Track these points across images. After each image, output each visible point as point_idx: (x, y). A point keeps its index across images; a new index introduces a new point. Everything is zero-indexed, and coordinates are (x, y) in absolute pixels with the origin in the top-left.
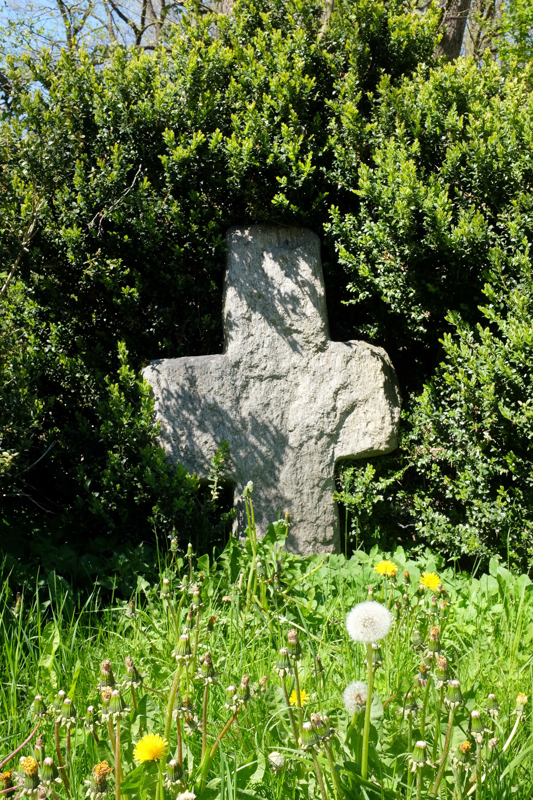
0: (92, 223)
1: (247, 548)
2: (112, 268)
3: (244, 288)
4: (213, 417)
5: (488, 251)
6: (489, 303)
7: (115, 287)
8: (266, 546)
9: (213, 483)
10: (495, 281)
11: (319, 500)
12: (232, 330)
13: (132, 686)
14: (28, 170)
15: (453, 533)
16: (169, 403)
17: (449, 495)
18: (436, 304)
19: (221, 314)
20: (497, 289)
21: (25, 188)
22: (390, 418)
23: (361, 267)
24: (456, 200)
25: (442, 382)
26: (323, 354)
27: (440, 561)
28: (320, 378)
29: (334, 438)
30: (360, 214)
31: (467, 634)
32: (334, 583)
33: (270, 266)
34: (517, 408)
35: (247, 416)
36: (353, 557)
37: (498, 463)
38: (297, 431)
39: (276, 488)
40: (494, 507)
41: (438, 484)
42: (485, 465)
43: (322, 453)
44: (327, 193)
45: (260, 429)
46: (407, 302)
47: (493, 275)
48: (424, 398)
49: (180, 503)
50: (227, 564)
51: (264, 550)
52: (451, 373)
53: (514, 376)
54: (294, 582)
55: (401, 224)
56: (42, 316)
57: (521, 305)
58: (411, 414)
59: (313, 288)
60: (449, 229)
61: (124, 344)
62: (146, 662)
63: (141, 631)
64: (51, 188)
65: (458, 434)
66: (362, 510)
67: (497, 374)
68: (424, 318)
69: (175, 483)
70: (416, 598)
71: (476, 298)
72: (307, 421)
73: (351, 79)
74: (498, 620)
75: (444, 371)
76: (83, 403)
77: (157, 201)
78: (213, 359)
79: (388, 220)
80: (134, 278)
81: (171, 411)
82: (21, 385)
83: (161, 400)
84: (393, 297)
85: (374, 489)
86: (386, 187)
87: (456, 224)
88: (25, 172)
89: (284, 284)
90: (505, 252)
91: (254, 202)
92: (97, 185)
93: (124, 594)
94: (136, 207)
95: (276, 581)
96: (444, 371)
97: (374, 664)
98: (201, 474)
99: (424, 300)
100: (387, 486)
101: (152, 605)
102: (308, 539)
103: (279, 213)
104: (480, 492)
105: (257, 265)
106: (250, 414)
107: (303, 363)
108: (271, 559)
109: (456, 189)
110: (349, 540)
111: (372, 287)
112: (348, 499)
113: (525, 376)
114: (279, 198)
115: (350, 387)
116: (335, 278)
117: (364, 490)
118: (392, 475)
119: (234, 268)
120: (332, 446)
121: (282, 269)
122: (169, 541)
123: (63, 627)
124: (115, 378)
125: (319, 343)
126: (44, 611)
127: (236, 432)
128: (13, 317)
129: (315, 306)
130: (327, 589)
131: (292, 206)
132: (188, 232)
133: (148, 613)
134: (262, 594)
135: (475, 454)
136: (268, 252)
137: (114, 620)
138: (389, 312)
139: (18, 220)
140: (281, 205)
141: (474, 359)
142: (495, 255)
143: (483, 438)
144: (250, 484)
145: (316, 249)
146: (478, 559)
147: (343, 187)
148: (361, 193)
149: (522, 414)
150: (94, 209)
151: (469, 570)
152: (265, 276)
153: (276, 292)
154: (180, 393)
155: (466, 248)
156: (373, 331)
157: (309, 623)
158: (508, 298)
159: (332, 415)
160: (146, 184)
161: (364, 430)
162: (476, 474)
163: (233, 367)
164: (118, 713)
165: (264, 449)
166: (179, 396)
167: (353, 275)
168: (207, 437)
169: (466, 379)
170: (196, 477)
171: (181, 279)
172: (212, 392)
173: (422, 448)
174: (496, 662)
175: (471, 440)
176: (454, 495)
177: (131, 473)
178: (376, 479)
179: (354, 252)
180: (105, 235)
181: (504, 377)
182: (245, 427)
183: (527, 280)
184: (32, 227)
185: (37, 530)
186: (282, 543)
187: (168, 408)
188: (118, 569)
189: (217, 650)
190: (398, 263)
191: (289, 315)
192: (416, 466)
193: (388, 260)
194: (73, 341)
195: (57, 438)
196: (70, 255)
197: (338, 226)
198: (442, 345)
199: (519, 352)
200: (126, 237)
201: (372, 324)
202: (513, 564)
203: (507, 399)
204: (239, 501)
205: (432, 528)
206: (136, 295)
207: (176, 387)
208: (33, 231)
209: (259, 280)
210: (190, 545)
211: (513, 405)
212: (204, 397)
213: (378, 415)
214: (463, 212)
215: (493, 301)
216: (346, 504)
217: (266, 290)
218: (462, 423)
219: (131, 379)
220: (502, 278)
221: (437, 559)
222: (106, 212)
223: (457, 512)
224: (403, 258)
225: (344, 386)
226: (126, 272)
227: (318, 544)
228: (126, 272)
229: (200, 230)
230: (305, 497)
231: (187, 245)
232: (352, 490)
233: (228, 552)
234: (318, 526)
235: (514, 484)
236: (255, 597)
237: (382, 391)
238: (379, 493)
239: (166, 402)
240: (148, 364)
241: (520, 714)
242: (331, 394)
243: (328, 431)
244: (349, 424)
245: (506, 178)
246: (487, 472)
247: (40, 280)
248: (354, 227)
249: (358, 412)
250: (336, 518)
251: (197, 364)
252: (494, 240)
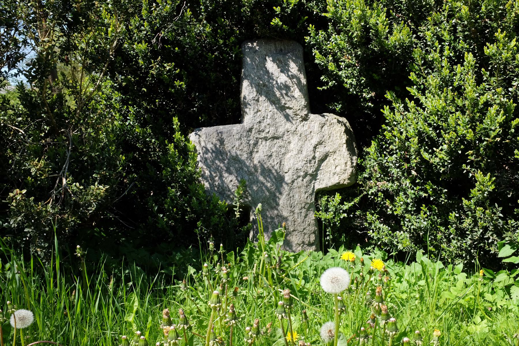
0: (154, 41)
1: (258, 247)
2: (168, 69)
3: (254, 81)
4: (236, 164)
5: (413, 51)
6: (414, 85)
7: (170, 81)
8: (271, 246)
9: (236, 207)
10: (418, 70)
11: (305, 217)
12: (247, 108)
13: (184, 327)
14: (111, 5)
15: (393, 237)
16: (207, 156)
17: (389, 212)
18: (378, 86)
19: (239, 98)
20: (419, 76)
21: (110, 18)
22: (350, 163)
23: (330, 64)
24: (391, 19)
25: (384, 139)
26: (306, 122)
27: (384, 255)
28: (305, 138)
29: (314, 176)
30: (329, 31)
31: (402, 300)
32: (316, 270)
33: (271, 66)
34: (433, 153)
35: (257, 163)
36: (328, 254)
37: (421, 190)
38: (290, 173)
39: (277, 210)
40: (419, 218)
41: (382, 206)
42: (413, 192)
43: (307, 187)
44: (306, 17)
45: (266, 172)
46: (360, 87)
47: (416, 67)
48: (372, 149)
49: (215, 219)
50: (246, 258)
51: (269, 248)
52: (390, 132)
53: (431, 132)
54: (289, 268)
55: (355, 35)
56: (124, 102)
57: (434, 85)
58: (364, 160)
60: (387, 38)
61: (177, 118)
62: (194, 318)
63: (191, 300)
64: (127, 17)
65: (394, 171)
66: (333, 223)
67: (419, 131)
68: (372, 96)
69: (211, 207)
70: (368, 276)
71: (405, 83)
72: (296, 166)
74: (423, 291)
75: (385, 130)
76: (151, 157)
77: (196, 25)
78: (235, 127)
79: (347, 32)
80: (182, 75)
81: (208, 161)
82: (111, 145)
83: (201, 154)
84: (351, 84)
85: (341, 209)
86: (344, 11)
87: (391, 34)
88: (110, 6)
89: (280, 77)
90: (424, 52)
91: (259, 24)
92: (157, 15)
93: (179, 277)
94: (183, 24)
95: (277, 267)
96: (385, 130)
97: (339, 309)
98: (228, 201)
99: (371, 85)
100: (349, 208)
101: (198, 283)
102: (299, 242)
103: (276, 31)
104: (410, 209)
105: (262, 65)
106: (259, 162)
107: (293, 129)
108: (275, 254)
109: (391, 11)
110: (325, 243)
111: (337, 78)
112: (324, 216)
113: (438, 131)
114: (276, 21)
115: (324, 143)
116: (313, 72)
117: (334, 210)
118: (353, 200)
119: (247, 67)
120: (313, 182)
121: (279, 67)
122: (208, 243)
123: (141, 299)
124: (171, 141)
125: (303, 115)
126: (128, 289)
127: (251, 174)
128: (105, 103)
129: (300, 91)
130: (311, 273)
131: (284, 26)
132: (217, 45)
133: (196, 289)
134: (269, 276)
135: (406, 185)
136: (269, 57)
137: (174, 294)
138: (349, 93)
139: (107, 39)
140: (277, 25)
141: (404, 122)
142: (417, 53)
143: (411, 174)
144: (260, 206)
145: (300, 54)
146: (409, 253)
147: (317, 13)
148: (329, 15)
149: (436, 156)
150: (155, 31)
151: (403, 261)
152: (268, 72)
153: (275, 82)
154: (214, 149)
155: (398, 49)
157: (300, 294)
158: (426, 81)
159: (313, 162)
160: (189, 13)
161: (333, 171)
162: (407, 197)
163: (248, 131)
164: (174, 340)
165: (269, 185)
166: (213, 151)
167: (325, 71)
168: (232, 177)
169: (399, 135)
170: (225, 203)
171: (213, 75)
172: (235, 148)
173: (372, 182)
174: (421, 316)
175: (403, 175)
176: (393, 212)
177: (183, 201)
178: (342, 203)
179: (325, 55)
180: (163, 48)
181: (423, 133)
182: (256, 171)
183: (438, 69)
184: (115, 42)
185: (124, 239)
186: (281, 243)
187: (206, 159)
188: (176, 262)
189: (240, 311)
190: (354, 61)
191: (283, 97)
192: (368, 194)
193: (347, 59)
194: (144, 118)
195: (135, 181)
196: (141, 62)
197: (314, 38)
198: (384, 114)
199: (434, 116)
200: (177, 49)
201: (338, 103)
202: (432, 255)
203: (426, 147)
204: (253, 219)
205: (378, 234)
206: (184, 86)
207: (211, 146)
208: (116, 45)
209: (264, 75)
210: (221, 245)
211: (430, 151)
212: (230, 152)
213: (343, 161)
214: (395, 26)
215: (417, 84)
216: (323, 219)
217: (269, 82)
218: (397, 165)
219: (182, 141)
220: (422, 68)
221: (383, 254)
222: (163, 33)
223: (395, 223)
224: (357, 57)
225: (320, 143)
226: (177, 72)
227: (305, 246)
228: (177, 72)
229: (224, 43)
230: (296, 215)
231: (216, 53)
232: (327, 210)
233: (247, 250)
234: (305, 234)
235: (432, 203)
236: (265, 278)
237: (345, 146)
238: (344, 212)
239: (205, 155)
240: (193, 131)
241: (435, 342)
242: (312, 148)
243: (310, 172)
244: (324, 168)
245: (424, 3)
246: (414, 196)
247: (122, 79)
248: (325, 39)
250: (316, 229)
251: (224, 130)
252: (416, 44)
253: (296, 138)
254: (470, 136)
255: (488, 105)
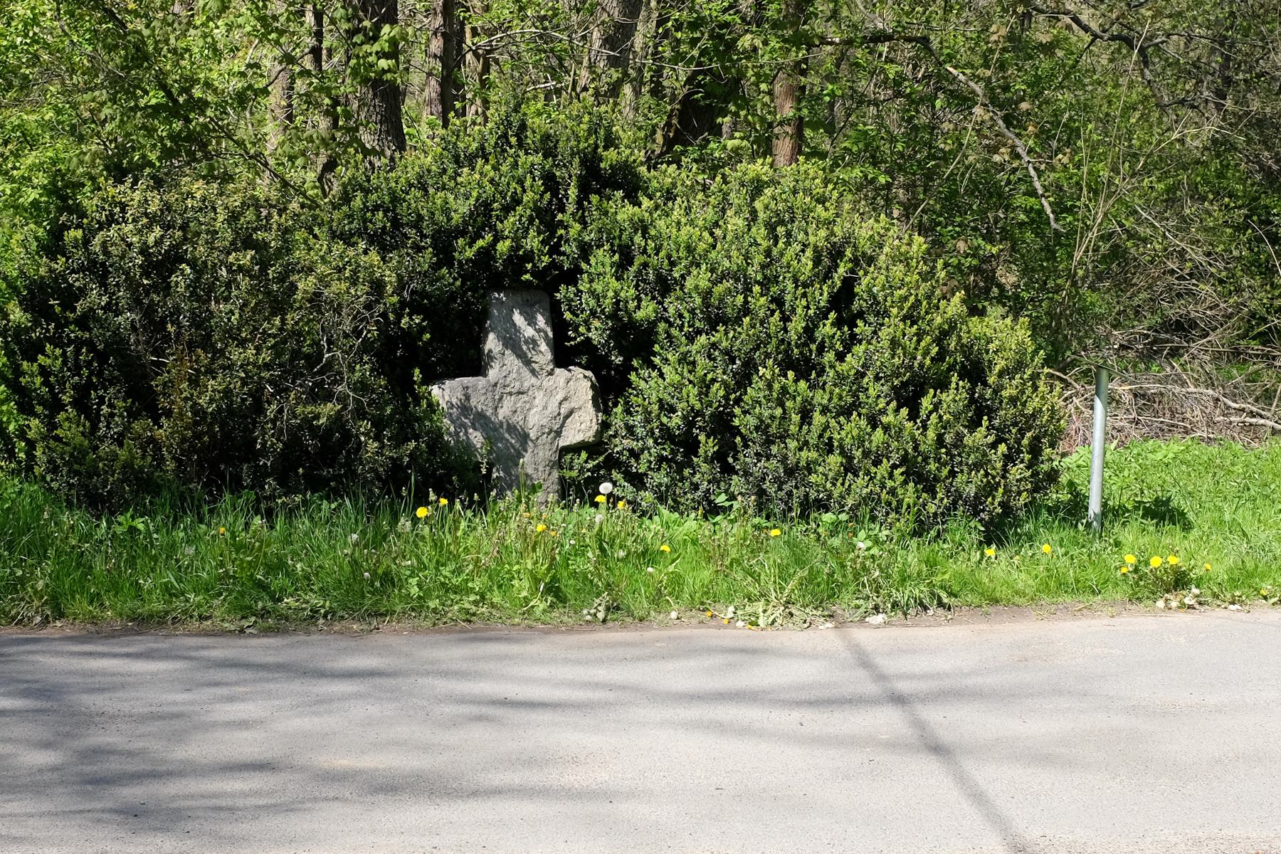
4: (481, 420)
28: (550, 393)
29: (558, 433)
33: (518, 318)
45: (511, 428)
48: (619, 409)
59: (546, 333)
65: (640, 431)
73: (573, 192)
112: (568, 474)
127: (495, 430)
141: (649, 386)
145: (547, 306)
156: (584, 360)
168: (478, 434)
182: (501, 426)
213: (588, 418)
223: (638, 481)
225: (565, 399)
249: (575, 415)
253: (542, 393)
254: (698, 406)
255: (714, 381)
